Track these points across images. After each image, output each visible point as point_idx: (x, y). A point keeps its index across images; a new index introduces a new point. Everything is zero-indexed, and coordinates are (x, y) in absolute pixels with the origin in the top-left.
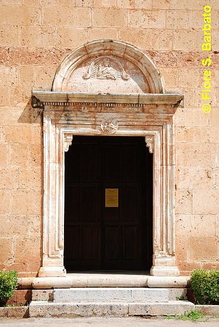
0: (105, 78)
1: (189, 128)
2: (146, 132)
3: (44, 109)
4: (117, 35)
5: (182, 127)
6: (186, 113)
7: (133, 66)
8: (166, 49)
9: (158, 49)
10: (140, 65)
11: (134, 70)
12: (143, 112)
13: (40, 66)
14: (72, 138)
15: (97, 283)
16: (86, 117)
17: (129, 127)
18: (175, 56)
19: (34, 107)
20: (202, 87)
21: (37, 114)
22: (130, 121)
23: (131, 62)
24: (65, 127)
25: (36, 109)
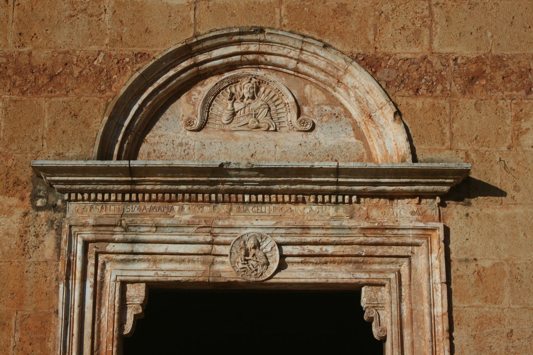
0: (209, 234)
1: (487, 264)
2: (362, 276)
3: (65, 211)
4: (277, 17)
5: (467, 260)
6: (476, 221)
7: (324, 97)
8: (417, 50)
9: (390, 49)
10: (341, 95)
11: (326, 108)
12: (351, 217)
13: (61, 99)
14: (143, 293)
15: (281, 63)
16: (180, 232)
17: (313, 260)
18: (438, 67)
19: (39, 209)
20: (519, 149)
21: (45, 228)
22: (316, 243)
23: (317, 86)
24: (120, 266)
25: (42, 214)
